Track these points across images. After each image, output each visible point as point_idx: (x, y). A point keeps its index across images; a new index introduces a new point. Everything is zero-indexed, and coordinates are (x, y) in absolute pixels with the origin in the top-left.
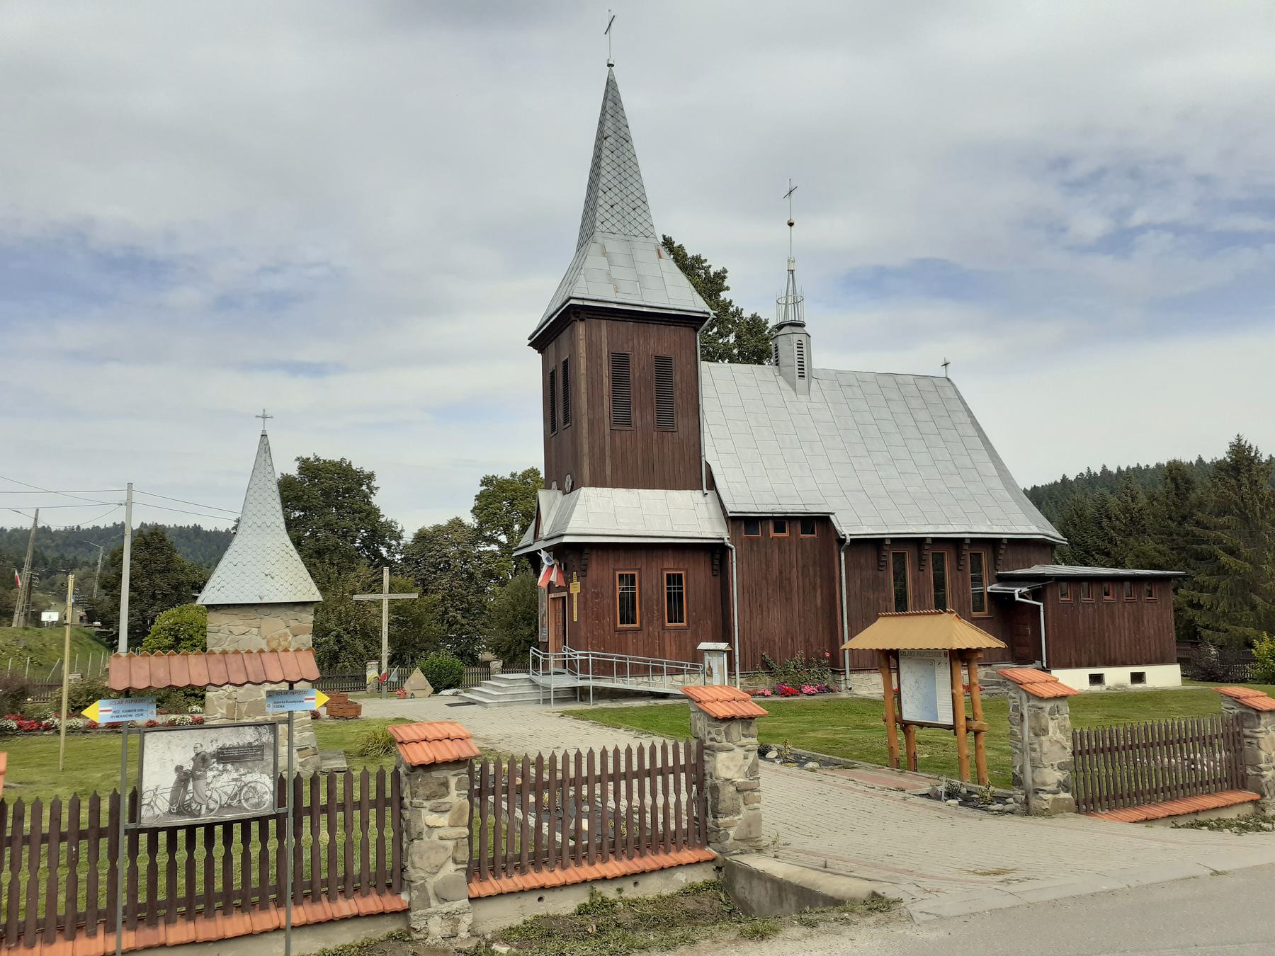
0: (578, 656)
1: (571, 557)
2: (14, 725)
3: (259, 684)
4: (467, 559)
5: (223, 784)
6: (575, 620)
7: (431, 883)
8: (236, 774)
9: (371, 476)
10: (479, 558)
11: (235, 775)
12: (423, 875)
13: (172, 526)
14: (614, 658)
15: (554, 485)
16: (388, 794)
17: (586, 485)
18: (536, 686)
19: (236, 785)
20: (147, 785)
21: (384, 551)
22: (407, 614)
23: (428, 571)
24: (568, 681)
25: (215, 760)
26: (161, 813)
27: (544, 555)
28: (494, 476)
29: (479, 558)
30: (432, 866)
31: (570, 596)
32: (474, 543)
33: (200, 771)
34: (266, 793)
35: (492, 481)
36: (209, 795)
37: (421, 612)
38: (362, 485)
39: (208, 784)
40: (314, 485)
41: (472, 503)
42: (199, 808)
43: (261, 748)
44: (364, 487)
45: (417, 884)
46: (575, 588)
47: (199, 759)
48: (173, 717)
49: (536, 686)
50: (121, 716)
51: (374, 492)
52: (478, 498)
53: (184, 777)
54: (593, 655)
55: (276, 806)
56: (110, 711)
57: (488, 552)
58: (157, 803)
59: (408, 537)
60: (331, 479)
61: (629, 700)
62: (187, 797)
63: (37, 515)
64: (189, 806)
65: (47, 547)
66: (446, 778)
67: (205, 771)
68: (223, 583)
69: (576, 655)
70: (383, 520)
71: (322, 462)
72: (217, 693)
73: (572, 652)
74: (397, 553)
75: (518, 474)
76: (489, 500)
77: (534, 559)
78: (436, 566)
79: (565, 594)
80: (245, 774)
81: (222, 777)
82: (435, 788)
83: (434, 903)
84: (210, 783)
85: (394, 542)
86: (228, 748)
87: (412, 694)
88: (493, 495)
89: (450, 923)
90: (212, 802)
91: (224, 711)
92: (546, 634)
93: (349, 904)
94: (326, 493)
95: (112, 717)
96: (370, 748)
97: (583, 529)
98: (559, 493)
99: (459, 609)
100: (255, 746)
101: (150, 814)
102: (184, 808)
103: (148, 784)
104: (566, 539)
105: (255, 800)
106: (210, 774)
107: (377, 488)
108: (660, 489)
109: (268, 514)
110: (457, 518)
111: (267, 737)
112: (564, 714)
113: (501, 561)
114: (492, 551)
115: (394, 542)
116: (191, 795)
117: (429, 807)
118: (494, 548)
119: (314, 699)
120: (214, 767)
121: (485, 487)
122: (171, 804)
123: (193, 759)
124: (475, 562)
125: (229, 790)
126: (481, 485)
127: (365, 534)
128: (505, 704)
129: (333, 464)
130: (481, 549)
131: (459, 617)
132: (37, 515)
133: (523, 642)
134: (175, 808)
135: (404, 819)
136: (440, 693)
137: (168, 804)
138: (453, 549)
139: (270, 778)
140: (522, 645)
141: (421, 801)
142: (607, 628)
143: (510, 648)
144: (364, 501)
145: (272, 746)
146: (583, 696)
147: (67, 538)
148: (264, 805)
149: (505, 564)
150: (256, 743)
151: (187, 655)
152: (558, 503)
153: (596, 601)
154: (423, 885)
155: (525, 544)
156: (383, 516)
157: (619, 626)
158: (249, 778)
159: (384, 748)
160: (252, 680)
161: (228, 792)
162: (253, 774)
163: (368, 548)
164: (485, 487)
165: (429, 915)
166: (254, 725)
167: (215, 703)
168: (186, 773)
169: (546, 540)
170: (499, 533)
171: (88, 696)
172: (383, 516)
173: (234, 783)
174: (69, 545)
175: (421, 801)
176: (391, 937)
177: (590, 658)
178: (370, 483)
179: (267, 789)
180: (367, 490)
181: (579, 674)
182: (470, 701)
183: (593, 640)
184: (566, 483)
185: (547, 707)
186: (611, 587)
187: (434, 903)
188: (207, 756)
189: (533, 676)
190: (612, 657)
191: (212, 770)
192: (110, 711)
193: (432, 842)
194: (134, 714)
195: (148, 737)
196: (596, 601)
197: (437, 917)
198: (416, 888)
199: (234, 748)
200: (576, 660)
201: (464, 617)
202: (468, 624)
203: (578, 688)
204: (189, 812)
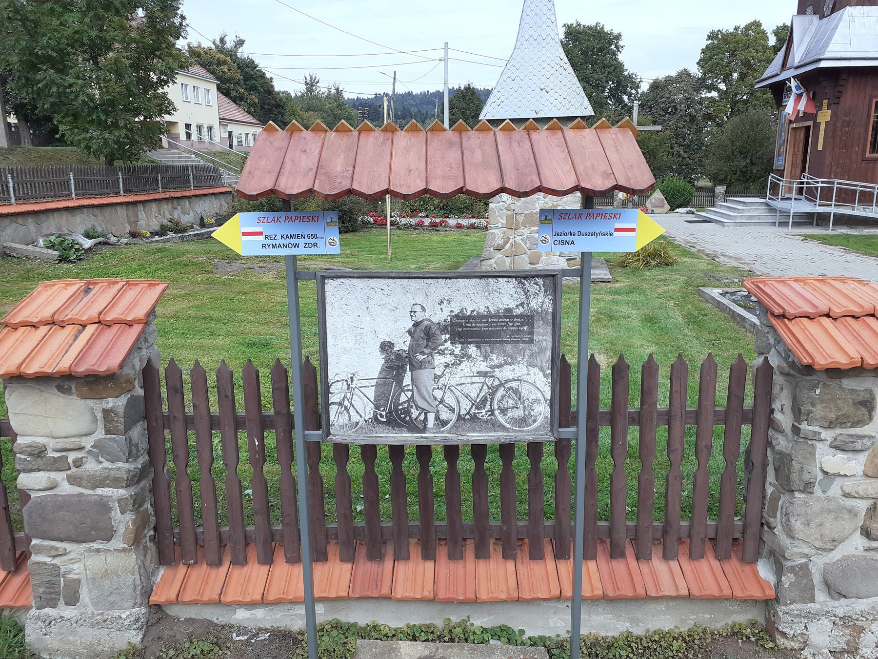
0: (820, 183)
1: (824, 84)
2: (371, 220)
3: (526, 194)
4: (691, 104)
5: (463, 380)
6: (820, 148)
7: (818, 565)
8: (484, 364)
9: (618, 37)
10: (700, 103)
11: (483, 367)
12: (806, 551)
13: (482, 89)
14: (859, 186)
15: (810, 9)
16: (748, 403)
17: (852, 4)
18: (772, 209)
19: (484, 383)
20: (336, 371)
21: (625, 98)
22: (645, 147)
23: (659, 114)
24: (806, 207)
25: (448, 336)
26: (361, 421)
27: (793, 84)
28: (719, 31)
29: (700, 103)
30: (827, 539)
31: (817, 125)
32: (697, 90)
33: (423, 353)
34: (537, 401)
35: (717, 35)
36: (439, 397)
37: (656, 145)
38: (611, 45)
39: (437, 378)
40: (576, 47)
41: (698, 56)
42: (422, 417)
43: (529, 319)
44: (613, 47)
45: (794, 563)
46: (825, 116)
47: (419, 333)
48: (473, 221)
49: (772, 209)
50: (280, 246)
51: (620, 50)
52: (704, 51)
53: (396, 363)
54: (838, 183)
55: (556, 425)
56: (260, 234)
57: (709, 98)
58: (353, 403)
59: (644, 87)
60: (589, 40)
61: (869, 228)
62: (403, 398)
63: (395, 75)
64: (407, 412)
65: (412, 105)
66: (871, 392)
67: (430, 354)
68: (502, 99)
69: (818, 182)
70: (626, 73)
71: (582, 27)
72: (498, 204)
73: (811, 179)
74: (636, 100)
75: (741, 27)
76: (714, 52)
77: (779, 90)
78: (665, 110)
79: (810, 123)
80: (501, 366)
81: (460, 368)
82: (847, 408)
83: (820, 596)
84: (440, 377)
85: (634, 91)
86: (469, 317)
87: (653, 211)
88: (718, 47)
89: (848, 632)
90: (446, 410)
91: (504, 222)
92: (783, 163)
93: (670, 568)
94: (584, 53)
95: (264, 246)
96: (631, 261)
97: (843, 53)
98: (816, 18)
99: (682, 146)
100: (517, 316)
101: (343, 419)
102: (398, 416)
103: (337, 369)
104: (823, 64)
105: (519, 413)
106: (439, 360)
107: (622, 47)
108: (857, 5)
109: (544, 26)
110: (685, 70)
111: (541, 301)
112: (806, 238)
113: (720, 105)
114: (712, 97)
115: (634, 91)
116: (409, 394)
117: (829, 440)
118: (714, 94)
119: (633, 230)
120: (446, 349)
121: (710, 41)
122: (377, 407)
123: (409, 332)
124: (698, 107)
125: (473, 391)
126: (707, 40)
127: (612, 85)
128: (742, 224)
129: (591, 28)
130: (703, 96)
131: (682, 152)
132: (395, 75)
133: (738, 171)
134: (384, 413)
135: (773, 448)
136: (675, 211)
137: (372, 406)
138: (681, 96)
139: (545, 375)
140: (737, 174)
141: (817, 429)
142: (854, 157)
143: (726, 176)
144: (612, 57)
145: (550, 317)
146: (819, 222)
147: (422, 99)
148: (535, 421)
149: (723, 108)
150: (520, 311)
151: (393, 131)
152: (813, 29)
153: (847, 129)
154: (804, 568)
155: (770, 75)
156: (626, 70)
157: (868, 155)
158: (506, 373)
159: (644, 261)
160: (510, 185)
161: (472, 395)
162: (516, 367)
163: (614, 96)
164: (710, 41)
165: (811, 616)
166: (516, 277)
167: (497, 213)
168: (398, 356)
169: (797, 68)
170: (719, 81)
171: (420, 202)
172: (626, 70)
173: (482, 379)
174: (423, 104)
175: (817, 429)
176: (735, 633)
177: (836, 185)
178: (618, 42)
179: (540, 396)
180: (615, 49)
181: (818, 200)
182: (707, 219)
183: (838, 168)
184: (826, 6)
185: (784, 230)
186: (865, 115)
187: (820, 596)
188: (434, 329)
189: (770, 201)
190: (856, 186)
191: (442, 353)
192: (260, 234)
193: (829, 500)
194: (301, 242)
195: (330, 286)
196: (847, 129)
197: (826, 622)
198: (792, 569)
199: (480, 316)
200: (817, 188)
201: (685, 152)
202: (688, 157)
203: (816, 214)
204: (406, 422)
